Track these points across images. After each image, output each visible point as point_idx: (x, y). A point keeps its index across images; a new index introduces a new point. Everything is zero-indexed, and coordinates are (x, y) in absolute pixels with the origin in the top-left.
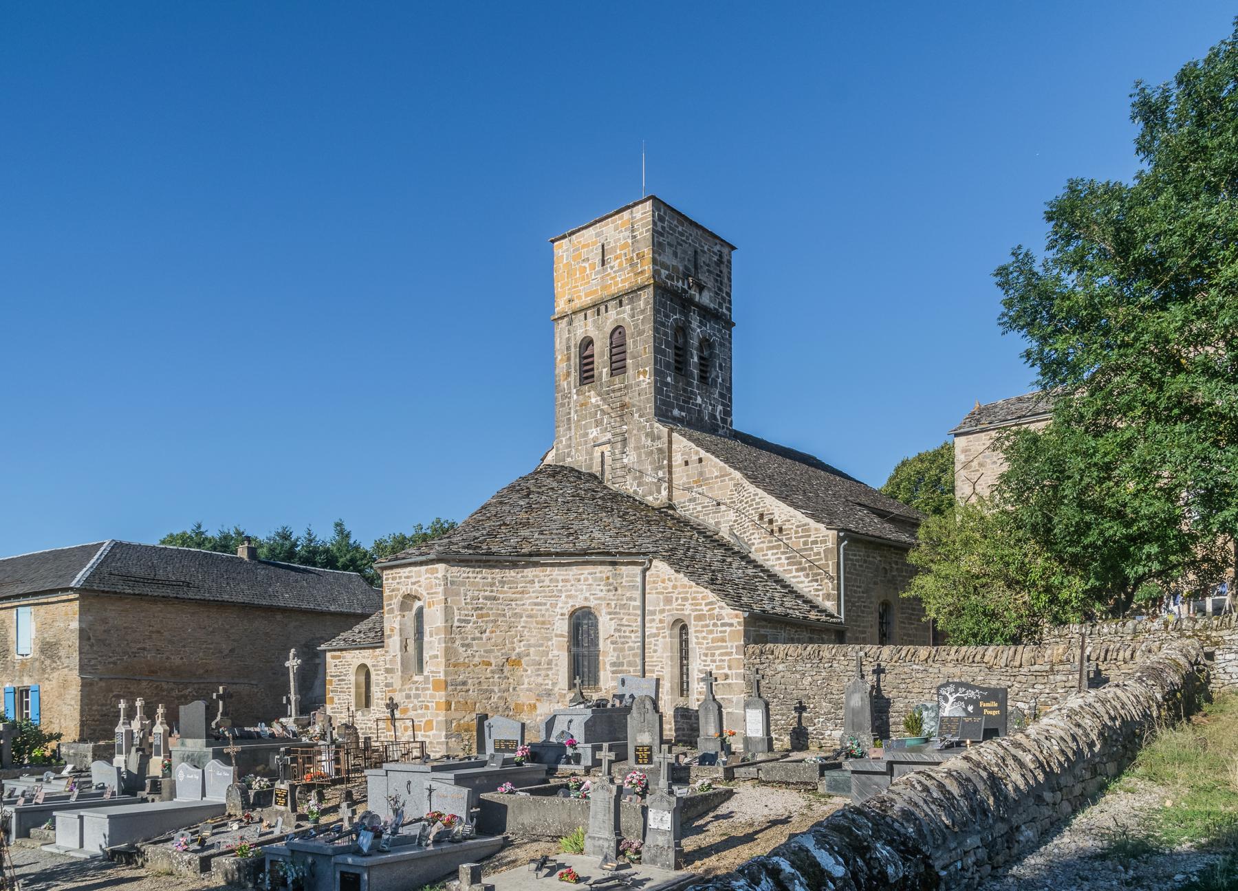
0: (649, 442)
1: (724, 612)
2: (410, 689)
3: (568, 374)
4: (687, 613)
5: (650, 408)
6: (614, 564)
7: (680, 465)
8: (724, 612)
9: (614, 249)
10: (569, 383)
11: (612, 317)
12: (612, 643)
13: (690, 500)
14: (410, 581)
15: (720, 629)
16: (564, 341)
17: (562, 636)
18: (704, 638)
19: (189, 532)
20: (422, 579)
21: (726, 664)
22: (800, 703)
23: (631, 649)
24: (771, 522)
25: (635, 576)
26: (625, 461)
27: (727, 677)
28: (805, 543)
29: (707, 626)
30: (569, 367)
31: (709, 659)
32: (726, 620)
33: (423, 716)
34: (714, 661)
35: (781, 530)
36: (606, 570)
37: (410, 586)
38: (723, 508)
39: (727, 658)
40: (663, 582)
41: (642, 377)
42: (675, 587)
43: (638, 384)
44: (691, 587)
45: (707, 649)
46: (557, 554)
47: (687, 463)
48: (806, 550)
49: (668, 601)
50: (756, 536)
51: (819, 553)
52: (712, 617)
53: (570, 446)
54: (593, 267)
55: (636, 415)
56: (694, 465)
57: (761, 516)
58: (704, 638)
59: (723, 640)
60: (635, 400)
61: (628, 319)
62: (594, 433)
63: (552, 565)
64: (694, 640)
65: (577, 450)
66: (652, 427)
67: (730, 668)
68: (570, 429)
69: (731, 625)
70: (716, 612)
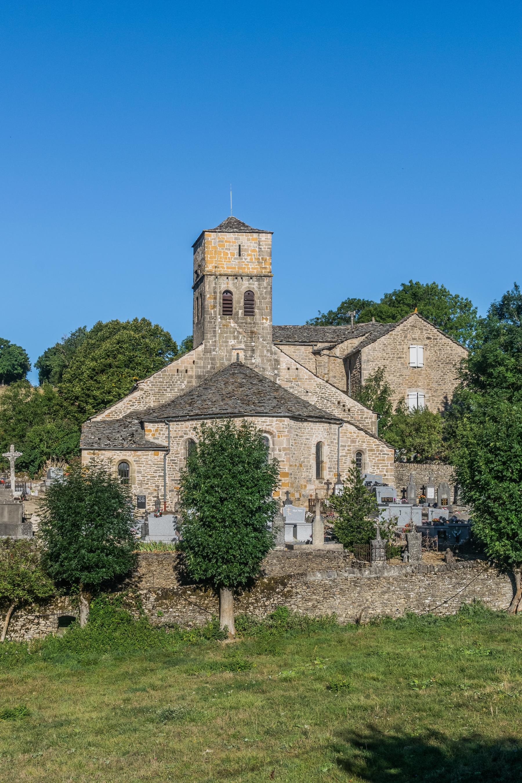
0: (269, 355)
1: (384, 449)
3: (214, 307)
4: (364, 448)
5: (270, 337)
6: (330, 423)
7: (285, 369)
8: (384, 449)
9: (246, 250)
10: (215, 312)
11: (245, 285)
12: (329, 458)
13: (290, 387)
15: (382, 456)
16: (212, 288)
17: (314, 454)
18: (373, 459)
21: (385, 470)
22: (423, 486)
23: (334, 461)
24: (344, 406)
25: (336, 429)
26: (253, 361)
27: (385, 475)
28: (362, 418)
30: (215, 303)
31: (376, 468)
32: (386, 452)
35: (349, 410)
36: (326, 425)
38: (310, 394)
39: (385, 468)
40: (351, 433)
41: (264, 321)
42: (358, 436)
43: (263, 324)
45: (375, 463)
46: (316, 417)
47: (289, 369)
48: (362, 421)
50: (336, 411)
51: (368, 423)
52: (378, 450)
53: (215, 346)
54: (233, 254)
55: (261, 340)
56: (293, 371)
57: (339, 403)
58: (373, 459)
59: (384, 460)
60: (261, 331)
61: (256, 289)
62: (232, 342)
63: (311, 421)
65: (220, 349)
66: (271, 347)
67: (387, 472)
68: (215, 336)
69: (388, 454)
70: (380, 448)
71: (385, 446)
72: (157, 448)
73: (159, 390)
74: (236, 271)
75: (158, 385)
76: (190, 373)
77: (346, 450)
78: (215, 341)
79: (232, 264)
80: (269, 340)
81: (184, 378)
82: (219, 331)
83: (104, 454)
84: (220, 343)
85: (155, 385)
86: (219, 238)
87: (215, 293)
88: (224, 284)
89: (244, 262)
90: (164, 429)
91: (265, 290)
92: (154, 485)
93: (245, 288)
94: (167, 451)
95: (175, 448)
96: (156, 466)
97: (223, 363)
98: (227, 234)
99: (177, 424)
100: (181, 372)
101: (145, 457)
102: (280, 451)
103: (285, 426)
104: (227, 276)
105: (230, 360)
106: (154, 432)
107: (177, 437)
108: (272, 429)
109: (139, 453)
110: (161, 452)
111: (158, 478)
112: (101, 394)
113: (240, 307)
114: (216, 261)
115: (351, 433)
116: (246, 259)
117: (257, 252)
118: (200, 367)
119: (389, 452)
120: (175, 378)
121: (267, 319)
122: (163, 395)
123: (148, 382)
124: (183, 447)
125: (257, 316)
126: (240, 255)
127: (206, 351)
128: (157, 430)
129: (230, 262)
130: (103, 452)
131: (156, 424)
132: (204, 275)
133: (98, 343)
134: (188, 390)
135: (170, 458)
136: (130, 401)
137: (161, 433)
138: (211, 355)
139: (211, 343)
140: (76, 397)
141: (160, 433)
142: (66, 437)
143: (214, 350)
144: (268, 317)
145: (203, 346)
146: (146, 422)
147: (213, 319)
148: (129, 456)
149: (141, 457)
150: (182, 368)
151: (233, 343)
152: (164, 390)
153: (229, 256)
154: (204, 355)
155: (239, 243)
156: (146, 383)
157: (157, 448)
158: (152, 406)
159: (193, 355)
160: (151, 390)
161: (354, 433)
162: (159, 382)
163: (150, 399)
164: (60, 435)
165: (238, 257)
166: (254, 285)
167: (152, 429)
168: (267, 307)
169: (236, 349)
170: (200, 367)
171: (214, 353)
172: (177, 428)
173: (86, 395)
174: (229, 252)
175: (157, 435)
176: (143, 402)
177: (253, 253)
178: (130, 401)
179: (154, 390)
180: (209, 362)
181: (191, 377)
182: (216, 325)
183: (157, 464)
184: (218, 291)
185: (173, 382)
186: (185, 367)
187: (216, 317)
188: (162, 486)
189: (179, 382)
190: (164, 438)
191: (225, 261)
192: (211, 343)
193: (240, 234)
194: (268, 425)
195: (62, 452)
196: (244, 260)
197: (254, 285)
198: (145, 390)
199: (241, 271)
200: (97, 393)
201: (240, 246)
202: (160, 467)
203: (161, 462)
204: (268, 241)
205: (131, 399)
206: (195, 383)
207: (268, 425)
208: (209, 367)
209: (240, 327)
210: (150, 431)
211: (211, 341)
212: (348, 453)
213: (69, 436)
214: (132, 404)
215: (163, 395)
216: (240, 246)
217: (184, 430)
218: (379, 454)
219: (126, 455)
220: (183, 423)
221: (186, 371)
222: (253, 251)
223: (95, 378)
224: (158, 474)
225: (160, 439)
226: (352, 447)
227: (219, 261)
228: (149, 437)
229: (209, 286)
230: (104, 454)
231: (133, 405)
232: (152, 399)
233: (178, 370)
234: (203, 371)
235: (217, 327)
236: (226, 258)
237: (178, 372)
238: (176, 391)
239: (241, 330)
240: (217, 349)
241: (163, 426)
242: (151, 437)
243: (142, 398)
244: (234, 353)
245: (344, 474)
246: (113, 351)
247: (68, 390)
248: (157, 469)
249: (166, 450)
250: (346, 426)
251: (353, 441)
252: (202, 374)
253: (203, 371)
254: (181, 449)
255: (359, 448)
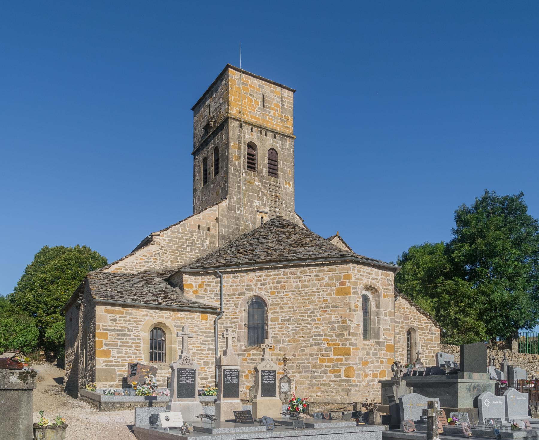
2: (370, 349)
3: (239, 158)
4: (416, 325)
11: (269, 141)
14: (371, 276)
16: (236, 136)
18: (423, 338)
19: (528, 213)
20: (379, 278)
21: (433, 351)
29: (425, 333)
30: (240, 154)
32: (433, 332)
33: (379, 367)
34: (428, 349)
37: (370, 280)
39: (433, 348)
40: (404, 308)
41: (287, 186)
42: (410, 312)
43: (286, 189)
44: (417, 314)
45: (424, 343)
49: (406, 318)
53: (239, 204)
55: (284, 206)
58: (423, 338)
59: (432, 340)
62: (257, 203)
64: (419, 339)
65: (245, 209)
68: (240, 193)
70: (429, 327)
71: (433, 325)
72: (207, 310)
73: (178, 247)
74: (260, 122)
75: (176, 241)
76: (212, 232)
77: (400, 327)
78: (240, 198)
79: (256, 114)
80: (291, 208)
81: (206, 236)
82: (244, 188)
83: (131, 314)
84: (244, 201)
85: (172, 241)
86: (243, 80)
87: (239, 141)
88: (249, 134)
89: (267, 115)
90: (213, 284)
91: (288, 152)
92: (202, 362)
93: (269, 144)
94: (219, 314)
95: (230, 310)
96: (205, 335)
97: (248, 226)
98: (251, 77)
99: (234, 277)
100: (203, 229)
101: (189, 321)
102: (386, 316)
103: (390, 282)
104: (252, 125)
105: (255, 224)
106: (195, 287)
107: (235, 295)
108: (378, 284)
109: (182, 314)
110: (211, 316)
111: (207, 352)
112: (51, 300)
113: (264, 164)
114: (240, 105)
115: (404, 308)
116: (270, 112)
117: (279, 107)
118: (224, 226)
119: (436, 331)
120: (196, 235)
121: (289, 184)
122: (183, 254)
123: (165, 236)
124: (243, 309)
125: (281, 179)
126: (264, 106)
127: (230, 208)
128: (200, 286)
129: (254, 111)
130: (130, 310)
131: (200, 277)
132: (227, 120)
133: (47, 261)
134: (210, 252)
135: (223, 324)
136: (144, 256)
137: (209, 289)
138: (236, 214)
139: (235, 200)
140: (28, 302)
141: (206, 290)
142: (24, 331)
143: (239, 209)
144: (291, 183)
145: (227, 201)
146: (185, 273)
147: (237, 172)
148: (167, 318)
149: (183, 321)
150: (204, 225)
151: (257, 204)
152: (184, 248)
153: (253, 103)
154: (228, 212)
155: (263, 92)
156: (163, 236)
157: (207, 310)
158: (169, 266)
159: (215, 211)
160: (169, 246)
161: (407, 308)
162: (178, 238)
163: (167, 257)
164: (18, 328)
165: (262, 107)
166: (278, 144)
167: (194, 284)
168: (290, 171)
169: (260, 212)
170: (224, 226)
171: (239, 212)
172: (233, 282)
173: (37, 301)
174: (253, 99)
175: (201, 292)
176: (160, 259)
177: (276, 108)
178: (144, 256)
179: (172, 247)
180: (233, 222)
181: (213, 236)
182: (240, 180)
183: (205, 332)
184: (243, 141)
185: (193, 240)
186: (207, 223)
187: (240, 170)
188: (212, 363)
189: (200, 241)
190: (213, 296)
191: (249, 108)
192: (235, 200)
193: (264, 82)
194: (373, 279)
195: (21, 344)
196: (267, 113)
197: (278, 144)
198: (161, 245)
199: (265, 125)
200: (47, 299)
201: (263, 96)
202: (210, 337)
203: (210, 329)
204: (290, 99)
205: (145, 254)
206: (218, 245)
207: (373, 279)
208: (234, 227)
209: (264, 187)
210: (191, 286)
211: (235, 197)
212: (401, 331)
213: (27, 330)
214: (146, 260)
215: (183, 254)
216: (263, 96)
217: (245, 284)
218: (428, 333)
219: (162, 317)
220: (244, 274)
221: (209, 229)
222: (276, 105)
223: (45, 287)
224: (207, 347)
225: (206, 298)
226: (404, 324)
227: (243, 106)
228: (189, 295)
229: (233, 132)
230: (131, 314)
231: (148, 262)
232: (169, 257)
233: (199, 226)
234: (228, 232)
235: (242, 183)
236: (250, 105)
237: (199, 229)
238: (197, 251)
239: (265, 191)
240: (242, 208)
241: (211, 280)
242: (192, 296)
243: (159, 254)
244: (259, 216)
245: (398, 354)
246: (62, 266)
247: (20, 298)
248: (206, 339)
249: (217, 312)
250: (399, 300)
251: (406, 318)
252: (226, 234)
253: (228, 232)
254: (240, 312)
255: (411, 325)
